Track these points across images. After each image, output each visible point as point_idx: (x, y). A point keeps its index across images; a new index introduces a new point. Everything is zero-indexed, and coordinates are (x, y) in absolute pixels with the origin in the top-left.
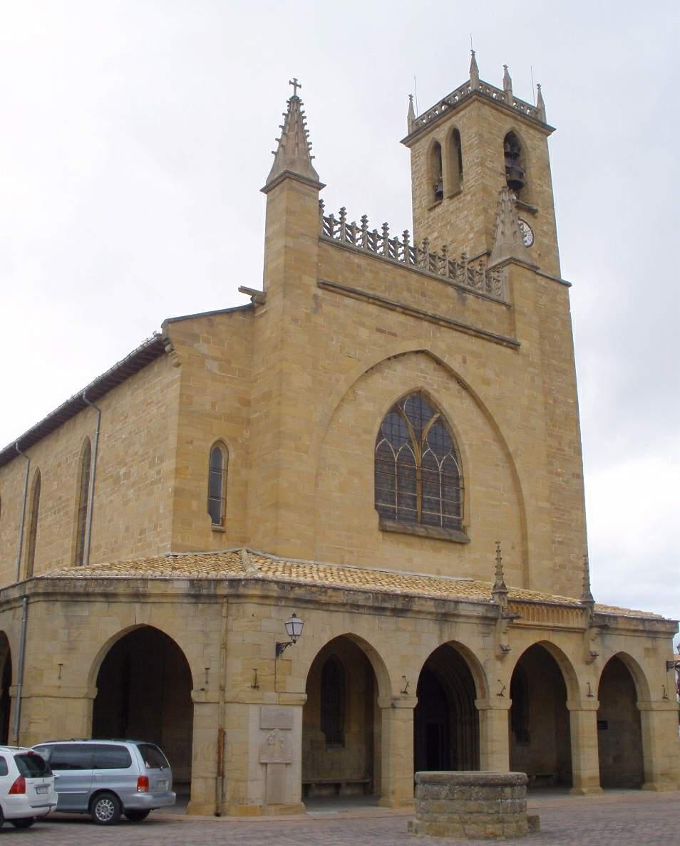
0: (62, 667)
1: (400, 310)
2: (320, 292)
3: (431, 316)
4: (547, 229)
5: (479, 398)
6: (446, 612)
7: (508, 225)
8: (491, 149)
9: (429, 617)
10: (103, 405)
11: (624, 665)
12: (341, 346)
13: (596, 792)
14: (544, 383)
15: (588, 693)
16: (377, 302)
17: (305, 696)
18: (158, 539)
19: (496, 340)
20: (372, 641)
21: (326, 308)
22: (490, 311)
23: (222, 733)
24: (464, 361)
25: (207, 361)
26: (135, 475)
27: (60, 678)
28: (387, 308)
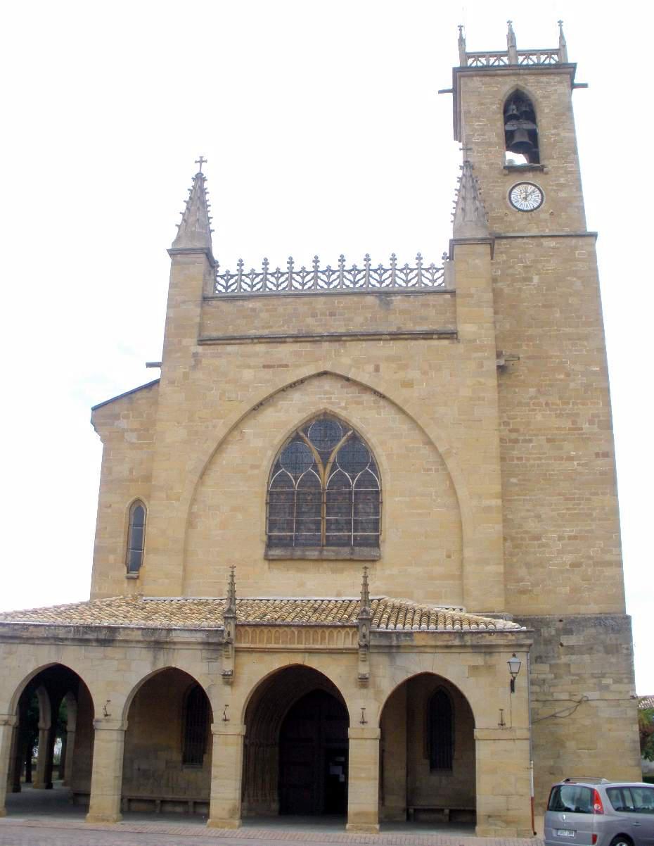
1: (291, 340)
2: (200, 349)
3: (327, 336)
6: (157, 641)
7: (469, 201)
9: (140, 645)
11: (39, 674)
15: (360, 720)
16: (264, 340)
19: (421, 336)
28: (278, 342)
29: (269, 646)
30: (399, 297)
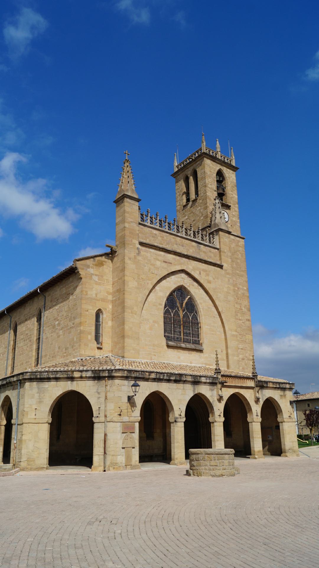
0: (36, 410)
2: (140, 247)
4: (235, 214)
5: (207, 290)
6: (196, 381)
8: (211, 179)
10: (47, 294)
12: (149, 269)
13: (261, 457)
14: (233, 281)
17: (140, 418)
18: (74, 352)
20: (166, 393)
21: (142, 253)
22: (210, 252)
23: (105, 435)
24: (200, 274)
25: (93, 276)
26: (63, 324)
27: (35, 415)
29: (231, 384)
30: (203, 246)
